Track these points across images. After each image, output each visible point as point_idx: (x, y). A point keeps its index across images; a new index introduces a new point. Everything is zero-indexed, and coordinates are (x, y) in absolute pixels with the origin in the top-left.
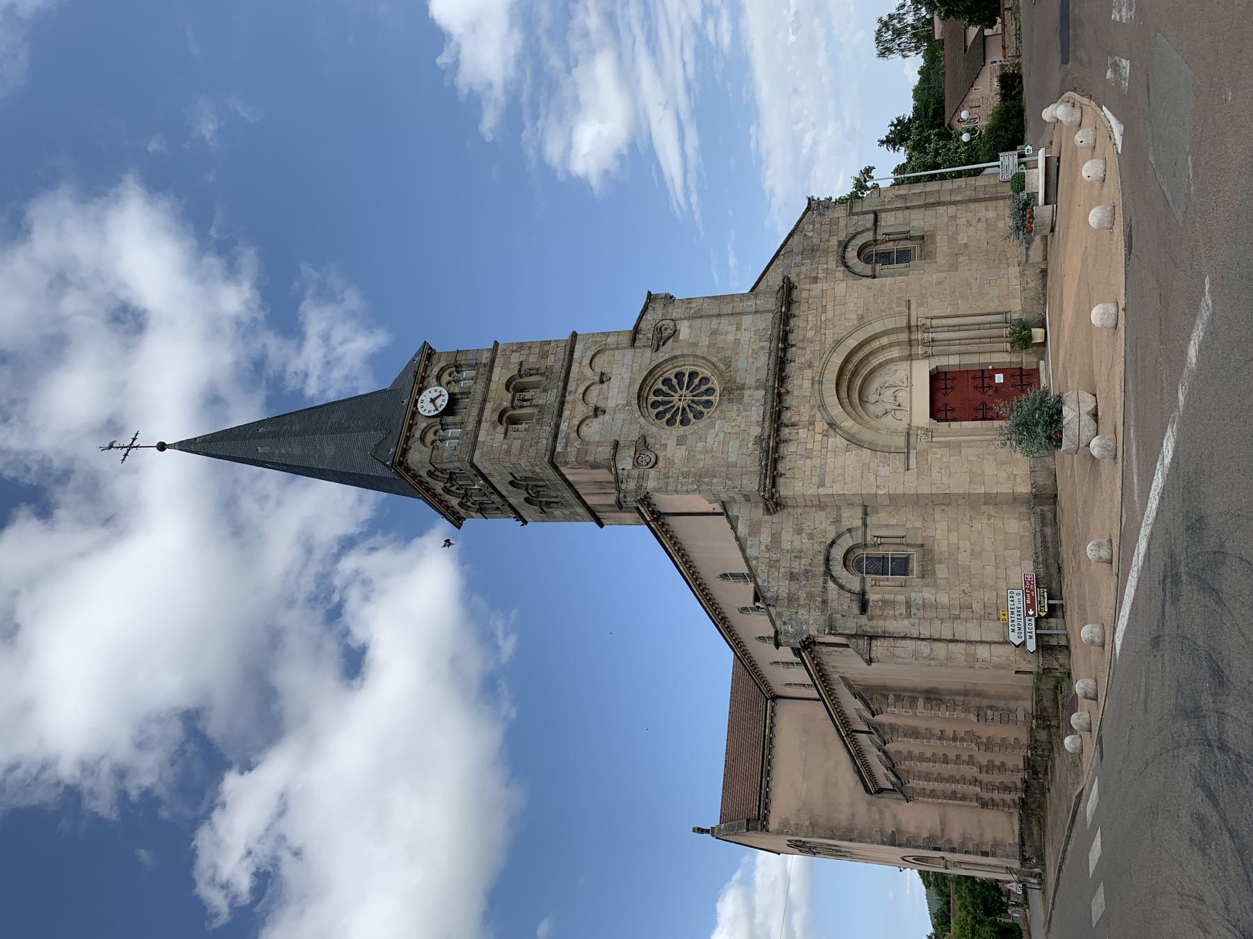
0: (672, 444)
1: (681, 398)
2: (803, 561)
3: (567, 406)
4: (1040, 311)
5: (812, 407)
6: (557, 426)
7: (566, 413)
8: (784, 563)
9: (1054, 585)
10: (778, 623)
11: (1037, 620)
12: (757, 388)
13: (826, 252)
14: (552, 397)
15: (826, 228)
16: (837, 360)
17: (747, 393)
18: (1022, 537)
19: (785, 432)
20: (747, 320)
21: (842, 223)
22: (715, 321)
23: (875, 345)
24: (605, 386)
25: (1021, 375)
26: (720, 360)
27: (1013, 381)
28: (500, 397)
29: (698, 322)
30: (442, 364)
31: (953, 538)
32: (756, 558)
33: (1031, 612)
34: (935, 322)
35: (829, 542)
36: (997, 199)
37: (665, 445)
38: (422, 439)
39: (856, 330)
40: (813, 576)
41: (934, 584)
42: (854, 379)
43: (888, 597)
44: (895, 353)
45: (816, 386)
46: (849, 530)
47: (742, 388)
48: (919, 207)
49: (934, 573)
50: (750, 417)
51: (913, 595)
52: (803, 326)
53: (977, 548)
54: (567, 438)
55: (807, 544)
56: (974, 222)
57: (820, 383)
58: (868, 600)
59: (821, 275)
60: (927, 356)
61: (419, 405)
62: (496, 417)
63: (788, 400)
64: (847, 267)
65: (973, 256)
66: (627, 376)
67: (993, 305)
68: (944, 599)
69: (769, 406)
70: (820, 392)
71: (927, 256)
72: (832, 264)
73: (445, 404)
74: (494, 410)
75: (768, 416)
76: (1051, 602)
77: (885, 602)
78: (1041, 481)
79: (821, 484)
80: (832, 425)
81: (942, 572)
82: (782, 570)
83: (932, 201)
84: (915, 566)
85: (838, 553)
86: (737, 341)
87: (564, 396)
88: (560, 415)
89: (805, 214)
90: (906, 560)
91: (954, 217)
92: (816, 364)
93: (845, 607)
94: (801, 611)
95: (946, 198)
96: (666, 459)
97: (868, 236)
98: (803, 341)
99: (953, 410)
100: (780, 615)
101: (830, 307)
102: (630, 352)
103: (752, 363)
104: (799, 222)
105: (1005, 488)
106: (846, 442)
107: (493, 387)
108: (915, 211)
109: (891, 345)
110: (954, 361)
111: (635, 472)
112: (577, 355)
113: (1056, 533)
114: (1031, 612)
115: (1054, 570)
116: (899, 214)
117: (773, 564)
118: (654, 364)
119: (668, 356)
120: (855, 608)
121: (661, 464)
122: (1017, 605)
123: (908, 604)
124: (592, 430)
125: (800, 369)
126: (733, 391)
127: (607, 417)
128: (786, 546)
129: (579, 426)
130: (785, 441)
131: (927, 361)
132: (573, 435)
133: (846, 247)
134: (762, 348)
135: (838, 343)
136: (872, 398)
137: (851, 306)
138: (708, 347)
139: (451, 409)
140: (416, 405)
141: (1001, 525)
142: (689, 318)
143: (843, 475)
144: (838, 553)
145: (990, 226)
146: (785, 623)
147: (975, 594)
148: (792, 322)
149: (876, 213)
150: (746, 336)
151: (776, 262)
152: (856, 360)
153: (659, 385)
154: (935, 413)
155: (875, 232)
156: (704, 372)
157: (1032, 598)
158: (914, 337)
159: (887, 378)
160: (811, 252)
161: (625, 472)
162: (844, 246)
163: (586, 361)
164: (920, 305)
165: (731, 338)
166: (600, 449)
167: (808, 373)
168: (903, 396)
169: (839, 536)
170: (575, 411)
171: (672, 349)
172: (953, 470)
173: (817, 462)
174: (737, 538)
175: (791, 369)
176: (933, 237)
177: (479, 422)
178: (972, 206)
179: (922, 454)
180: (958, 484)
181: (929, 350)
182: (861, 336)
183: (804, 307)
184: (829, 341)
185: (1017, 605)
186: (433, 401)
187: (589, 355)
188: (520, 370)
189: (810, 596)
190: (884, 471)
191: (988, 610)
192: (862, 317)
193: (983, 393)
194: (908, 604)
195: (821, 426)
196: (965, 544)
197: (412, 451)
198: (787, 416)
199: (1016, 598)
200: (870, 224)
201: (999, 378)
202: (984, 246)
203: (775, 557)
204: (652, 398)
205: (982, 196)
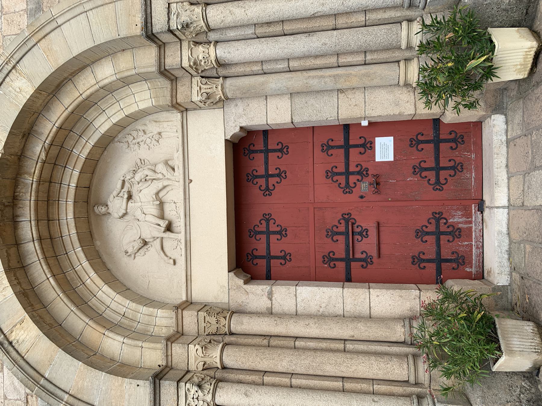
23: (86, 85)
25: (437, 142)
27: (415, 157)
39: (26, 47)
44: (141, 98)
60: (211, 102)
99: (282, 233)
106: (23, 390)
109: (125, 82)
110: (275, 114)
131: (218, 113)
136: (116, 205)
152: (48, 127)
154: (247, 260)
158: (172, 60)
159: (143, 153)
181: (216, 89)
182: (39, 68)
193: (348, 189)
201: (384, 149)
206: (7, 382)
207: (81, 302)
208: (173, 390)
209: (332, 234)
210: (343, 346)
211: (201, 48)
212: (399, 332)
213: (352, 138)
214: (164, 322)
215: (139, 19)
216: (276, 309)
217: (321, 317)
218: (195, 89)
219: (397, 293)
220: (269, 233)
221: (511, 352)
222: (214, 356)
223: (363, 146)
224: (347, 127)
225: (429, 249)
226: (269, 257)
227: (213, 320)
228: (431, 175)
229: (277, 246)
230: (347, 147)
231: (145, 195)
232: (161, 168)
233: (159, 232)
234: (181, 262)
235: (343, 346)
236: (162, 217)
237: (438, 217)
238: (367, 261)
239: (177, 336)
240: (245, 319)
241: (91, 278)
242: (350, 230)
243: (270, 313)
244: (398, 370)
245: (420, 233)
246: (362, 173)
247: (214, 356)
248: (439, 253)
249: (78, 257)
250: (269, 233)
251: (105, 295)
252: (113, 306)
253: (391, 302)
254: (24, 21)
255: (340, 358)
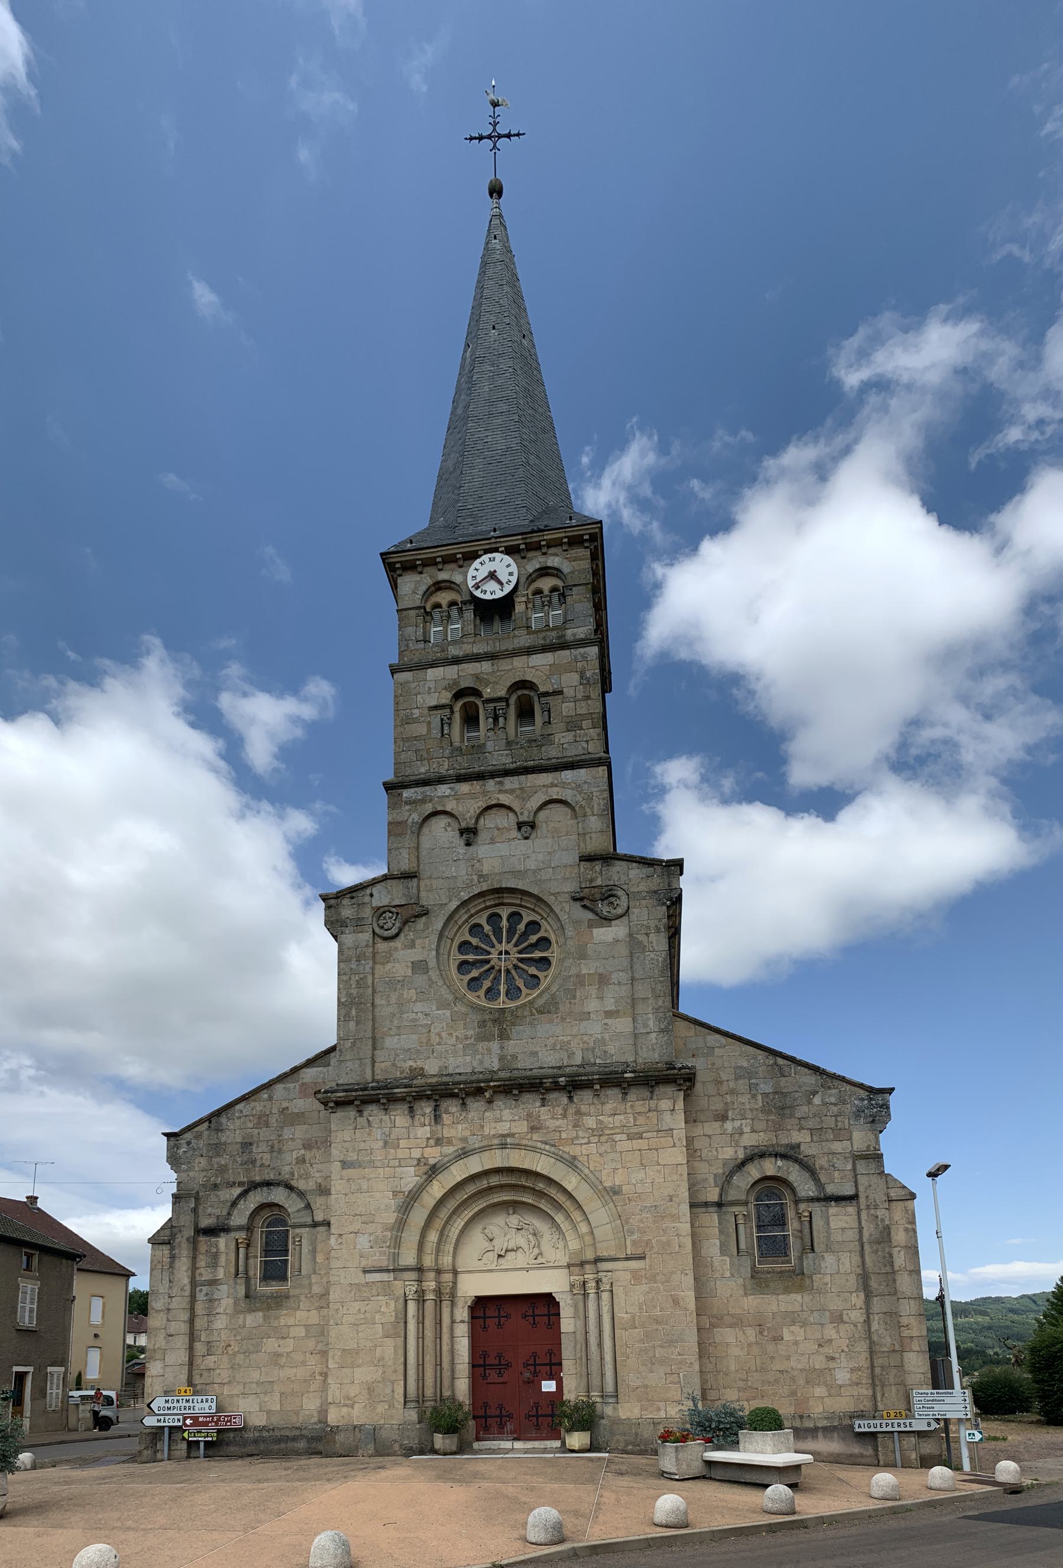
0: (415, 954)
1: (503, 954)
2: (267, 1156)
3: (476, 786)
4: (613, 1445)
5: (464, 1140)
6: (441, 780)
7: (464, 788)
8: (265, 1133)
9: (107, 1459)
10: (188, 1136)
11: (179, 1428)
12: (502, 1058)
13: (778, 1128)
14: (500, 758)
15: (830, 1122)
16: (542, 1165)
17: (495, 1046)
18: (297, 1413)
19: (428, 1108)
20: (623, 1025)
21: (838, 1147)
22: (624, 977)
24: (514, 833)
26: (553, 997)
28: (496, 680)
29: (623, 950)
30: (566, 567)
31: (301, 1332)
32: (270, 1098)
33: (188, 1422)
34: (605, 1296)
35: (294, 1183)
36: (874, 1385)
37: (412, 945)
38: (438, 586)
40: (248, 1170)
41: (237, 1312)
42: (516, 1191)
43: (222, 1259)
45: (496, 1141)
46: (308, 1206)
47: (503, 1036)
48: (863, 1263)
49: (251, 1311)
50: (455, 1055)
51: (224, 1288)
52: (609, 1111)
53: (283, 1361)
54: (423, 801)
55: (291, 1157)
56: (828, 1350)
57: (503, 1146)
58: (218, 1236)
59: (729, 1126)
61: (485, 558)
62: (465, 684)
63: (476, 1106)
64: (743, 1164)
65: (756, 1350)
66: (531, 864)
67: (631, 1378)
68: (220, 1323)
69: (458, 1078)
70: (489, 1148)
71: (758, 1282)
72: (750, 1140)
73: (488, 597)
74: (477, 677)
75: (446, 1079)
76: (202, 1445)
77: (216, 1256)
78: (340, 1438)
79: (345, 1164)
80: (434, 1171)
81: (253, 1320)
82: (256, 1131)
83: (873, 1284)
84: (273, 1288)
85: (278, 1196)
86: (586, 1016)
87: (493, 775)
88: (461, 778)
89: (861, 1086)
90: (283, 1278)
91: (838, 1319)
92: (535, 1137)
93: (209, 1210)
94: (203, 1161)
95: (877, 1304)
96: (390, 953)
97: (806, 1188)
98: (578, 1112)
100: (199, 1136)
101: (637, 1144)
102: (572, 858)
103: (540, 1046)
104: (843, 1079)
105: (334, 1392)
106: (407, 1189)
107: (518, 662)
108: (856, 1259)
110: (567, 1324)
111: (367, 913)
112: (567, 775)
113: (298, 1454)
114: (188, 1422)
115: (250, 1449)
116: (852, 1235)
117: (263, 1120)
118: (550, 900)
119: (564, 917)
120: (205, 1222)
121: (382, 946)
122: (198, 1406)
123: (213, 1282)
124: (442, 832)
125: (529, 1116)
126: (499, 1025)
127: (462, 849)
128: (287, 1133)
129: (445, 813)
130: (411, 1110)
132: (429, 808)
133: (784, 1156)
134: (571, 1055)
135: (572, 1163)
136: (514, 1220)
137: (638, 1175)
138: (578, 976)
139: (497, 611)
140: (487, 551)
141: (312, 1388)
142: (630, 935)
143: (359, 1190)
144: (278, 1196)
145: (814, 1376)
146: (189, 1143)
147: (225, 1358)
148: (614, 1093)
149: (853, 1198)
150: (594, 1028)
151: (761, 1055)
152: (552, 1192)
153: (527, 917)
154: (481, 1304)
155: (812, 1200)
156: (547, 979)
157: (206, 1424)
160: (780, 1107)
161: (367, 899)
162: (791, 1154)
163: (555, 793)
164: (635, 1274)
165: (593, 1005)
166: (405, 853)
167: (522, 1127)
168: (519, 1259)
169: (301, 1194)
170: (464, 801)
171: (577, 922)
172: (361, 1328)
173: (378, 1156)
174: (295, 1070)
175: (531, 1103)
176: (801, 1288)
177: (456, 661)
178: (862, 1347)
179: (386, 1289)
180: (342, 1336)
183: (640, 1106)
184: (575, 1150)
185: (198, 1406)
186: (492, 575)
187: (567, 795)
188: (546, 694)
189: (222, 1169)
190: (363, 1242)
191: (205, 1374)
192: (616, 1193)
193: (526, 1365)
194: (213, 1282)
195: (434, 1155)
196: (289, 1345)
197: (416, 577)
198: (452, 1106)
199: (206, 1405)
200: (831, 1189)
201: (549, 1386)
202: (778, 1366)
203: (273, 1120)
204: (505, 913)
205: (878, 1362)
206: (410, 1179)
207: (456, 1212)
208: (413, 1278)
209: (499, 1357)
210: (439, 1364)
211: (594, 1284)
212: (447, 1393)
213: (554, 1370)
214: (445, 1262)
215: (605, 1254)
216: (455, 1325)
217: (452, 1351)
218: (577, 1278)
219: (467, 1392)
220: (499, 1317)
221: (443, 1438)
222: (430, 1296)
223: (551, 1374)
224: (561, 1364)
225: (493, 1411)
226: (485, 1318)
227: (448, 1291)
228: (534, 1413)
229: (491, 1323)
230: (551, 1364)
231: (520, 1240)
232: (536, 1251)
233: (497, 1251)
234: (480, 1265)
235: (439, 1364)
236: (507, 1251)
237: (510, 1416)
238: (484, 1376)
239: (439, 1272)
240: (449, 1309)
241: (468, 1214)
242: (503, 1366)
243: (453, 1322)
244: (429, 1392)
245: (501, 1407)
246: (535, 1373)
247: (430, 1296)
248: (490, 1417)
249: (481, 1204)
250: (499, 1317)
251: (459, 1223)
252: (453, 1229)
253: (462, 1387)
254: (608, 1184)
255: (433, 1362)
